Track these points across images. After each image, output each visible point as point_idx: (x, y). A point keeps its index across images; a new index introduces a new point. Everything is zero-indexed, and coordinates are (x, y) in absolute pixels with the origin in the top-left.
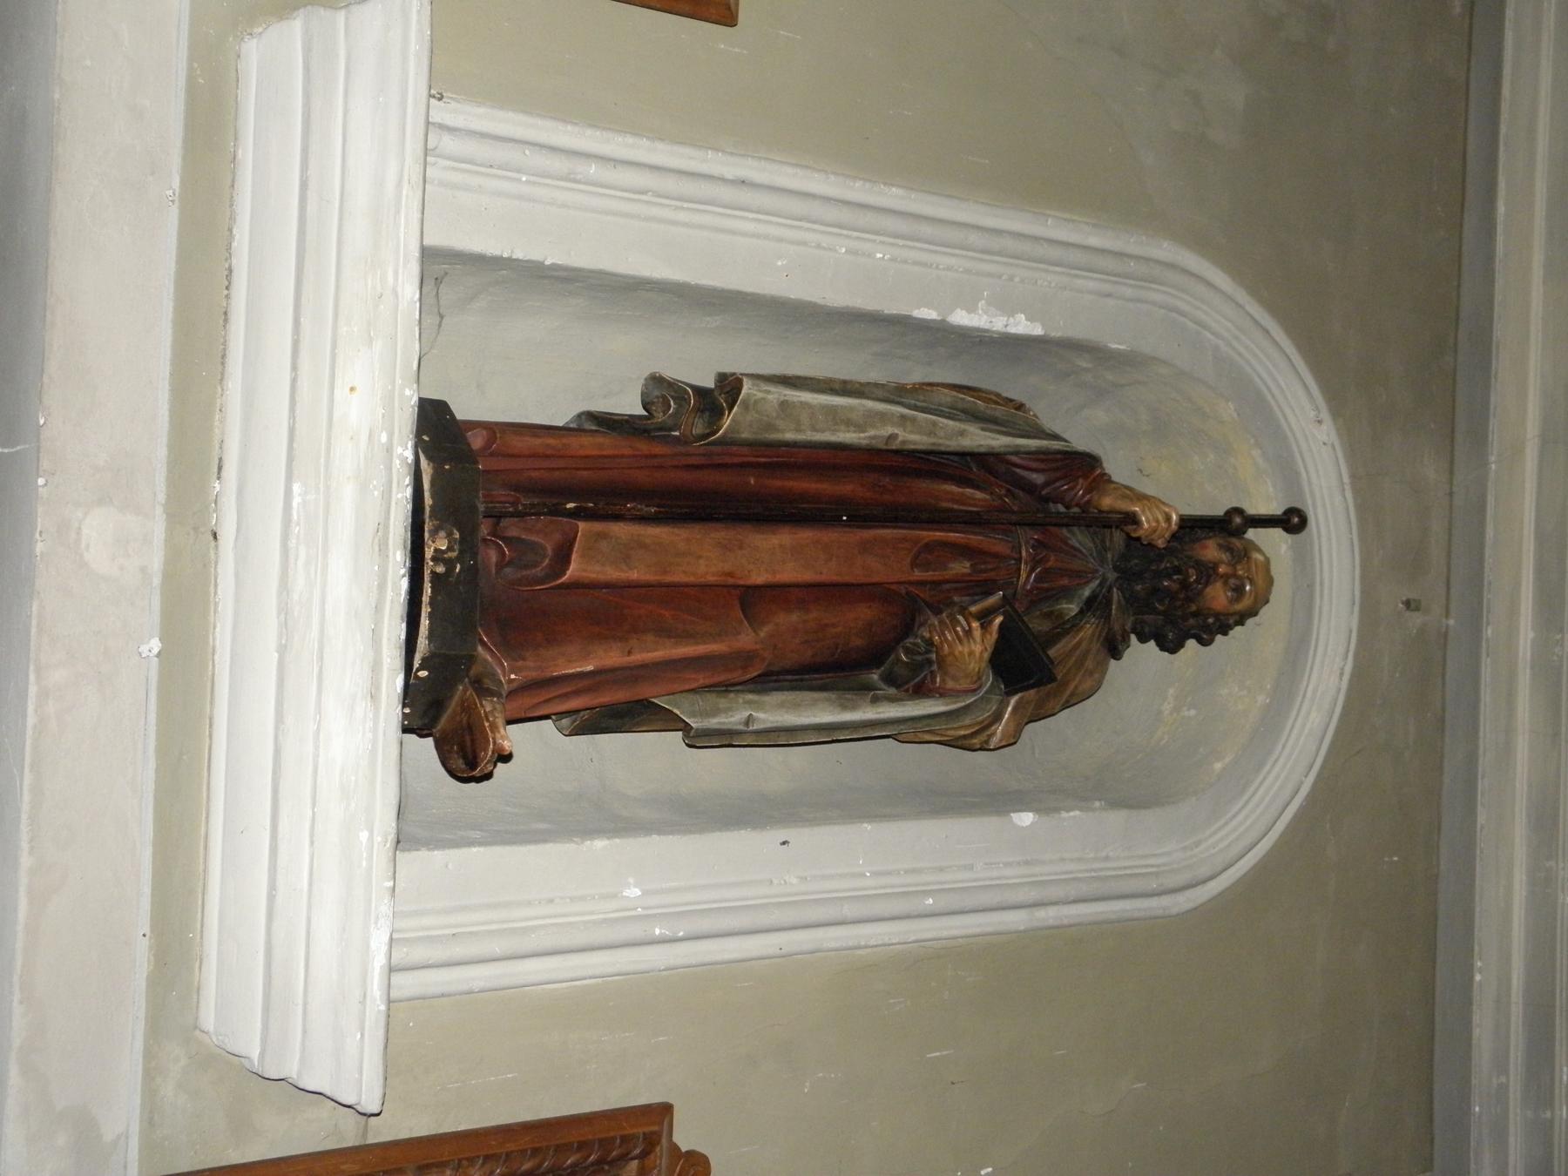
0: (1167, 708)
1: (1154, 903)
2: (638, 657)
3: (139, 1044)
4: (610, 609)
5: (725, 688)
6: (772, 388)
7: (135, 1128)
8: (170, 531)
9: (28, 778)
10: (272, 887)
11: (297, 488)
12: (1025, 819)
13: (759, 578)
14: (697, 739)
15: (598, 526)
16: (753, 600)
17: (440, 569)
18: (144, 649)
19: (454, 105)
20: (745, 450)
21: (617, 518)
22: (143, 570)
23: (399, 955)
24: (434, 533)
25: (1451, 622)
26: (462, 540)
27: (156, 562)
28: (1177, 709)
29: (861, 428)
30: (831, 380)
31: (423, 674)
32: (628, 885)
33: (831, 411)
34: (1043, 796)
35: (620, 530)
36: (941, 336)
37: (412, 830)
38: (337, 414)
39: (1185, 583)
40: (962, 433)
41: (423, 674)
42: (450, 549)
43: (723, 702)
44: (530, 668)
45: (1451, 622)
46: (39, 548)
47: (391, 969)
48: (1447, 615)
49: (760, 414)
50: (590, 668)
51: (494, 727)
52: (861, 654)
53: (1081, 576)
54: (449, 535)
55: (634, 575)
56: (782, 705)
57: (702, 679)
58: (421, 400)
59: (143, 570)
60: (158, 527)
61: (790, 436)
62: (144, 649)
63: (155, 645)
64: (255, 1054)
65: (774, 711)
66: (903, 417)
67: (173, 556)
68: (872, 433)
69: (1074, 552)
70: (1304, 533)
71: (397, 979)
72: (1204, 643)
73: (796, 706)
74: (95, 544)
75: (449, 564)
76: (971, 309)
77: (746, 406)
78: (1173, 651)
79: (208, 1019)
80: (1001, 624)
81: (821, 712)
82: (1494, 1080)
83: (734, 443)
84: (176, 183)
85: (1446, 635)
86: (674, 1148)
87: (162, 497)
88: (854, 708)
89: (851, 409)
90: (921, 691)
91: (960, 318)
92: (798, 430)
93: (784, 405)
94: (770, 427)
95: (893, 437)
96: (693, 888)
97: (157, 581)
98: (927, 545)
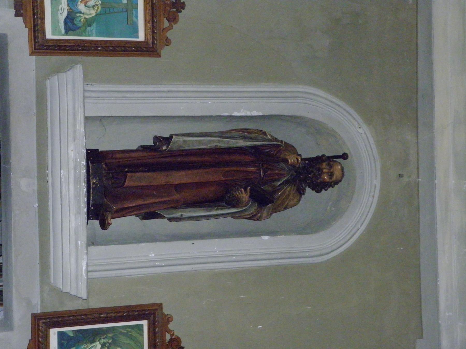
0: (329, 208)
1: (307, 259)
2: (146, 202)
3: (39, 286)
4: (139, 192)
5: (175, 208)
6: (181, 138)
7: (39, 303)
8: (38, 182)
9: (13, 232)
10: (62, 253)
11: (62, 171)
12: (266, 238)
13: (177, 182)
14: (171, 220)
15: (132, 174)
16: (179, 187)
17: (94, 186)
18: (35, 206)
19: (95, 86)
20: (179, 152)
21: (137, 172)
22: (33, 190)
23: (90, 268)
24: (93, 178)
25: (420, 180)
26: (99, 179)
27: (36, 188)
28: (331, 208)
29: (205, 144)
30: (202, 133)
31: (92, 208)
32: (151, 254)
33: (198, 141)
34: (272, 233)
35: (138, 174)
36: (231, 118)
37: (92, 242)
38: (69, 156)
39: (320, 173)
40: (237, 143)
41: (92, 208)
42: (96, 181)
43: (174, 211)
44: (120, 206)
45: (420, 180)
46: (12, 187)
47: (88, 271)
48: (418, 177)
49: (178, 143)
50: (134, 205)
51: (108, 220)
52: (218, 198)
53: (282, 175)
54: (96, 179)
55: (143, 184)
56: (190, 211)
57: (166, 207)
58: (87, 150)
59: (33, 190)
60: (36, 181)
61: (187, 148)
62: (35, 206)
63: (37, 205)
64: (61, 287)
65: (188, 213)
66: (219, 141)
67: (39, 186)
68: (210, 145)
69: (282, 169)
70: (347, 160)
71: (89, 274)
72: (326, 190)
73: (195, 211)
74: (22, 185)
75: (96, 185)
76: (239, 112)
77: (174, 143)
78: (318, 192)
79: (52, 281)
80: (250, 189)
81: (201, 212)
82: (447, 314)
83: (172, 151)
84: (35, 111)
85: (418, 184)
86: (162, 313)
87: (36, 175)
88: (210, 211)
89: (204, 140)
90: (234, 207)
91: (236, 114)
92: (189, 147)
93: (184, 141)
94: (181, 147)
95: (216, 145)
96: (169, 256)
97: (36, 192)
98: (226, 171)
